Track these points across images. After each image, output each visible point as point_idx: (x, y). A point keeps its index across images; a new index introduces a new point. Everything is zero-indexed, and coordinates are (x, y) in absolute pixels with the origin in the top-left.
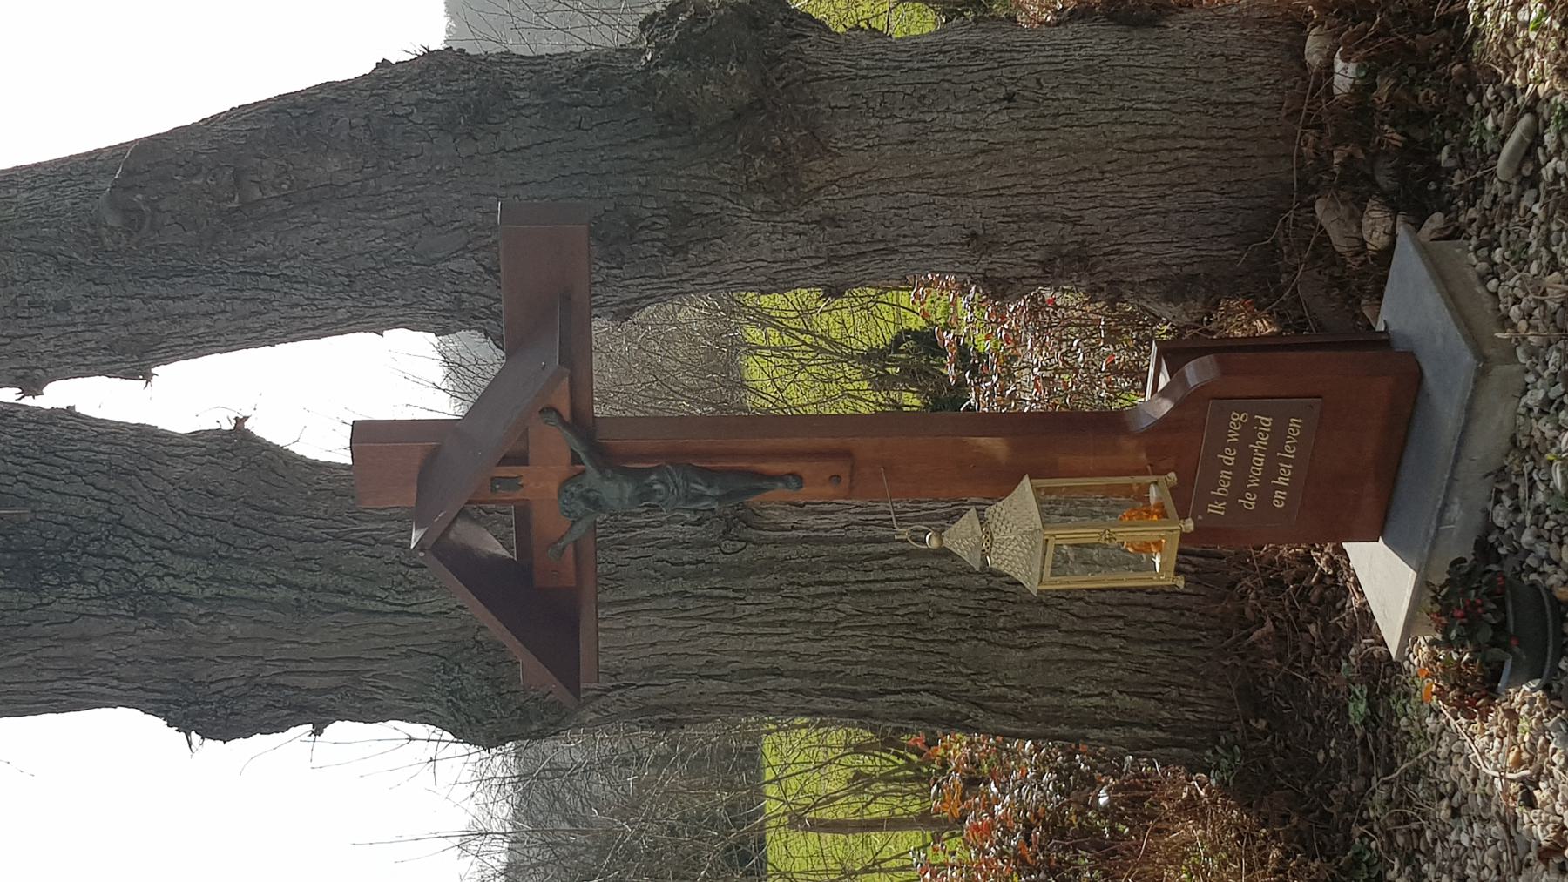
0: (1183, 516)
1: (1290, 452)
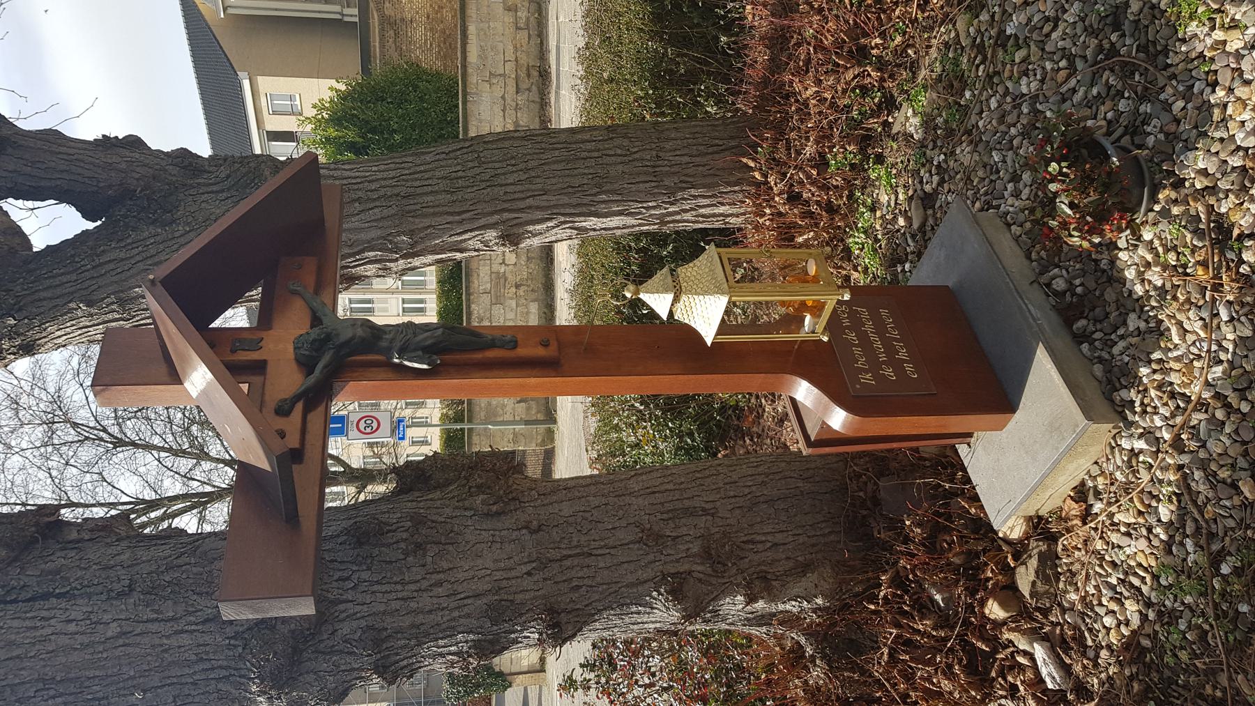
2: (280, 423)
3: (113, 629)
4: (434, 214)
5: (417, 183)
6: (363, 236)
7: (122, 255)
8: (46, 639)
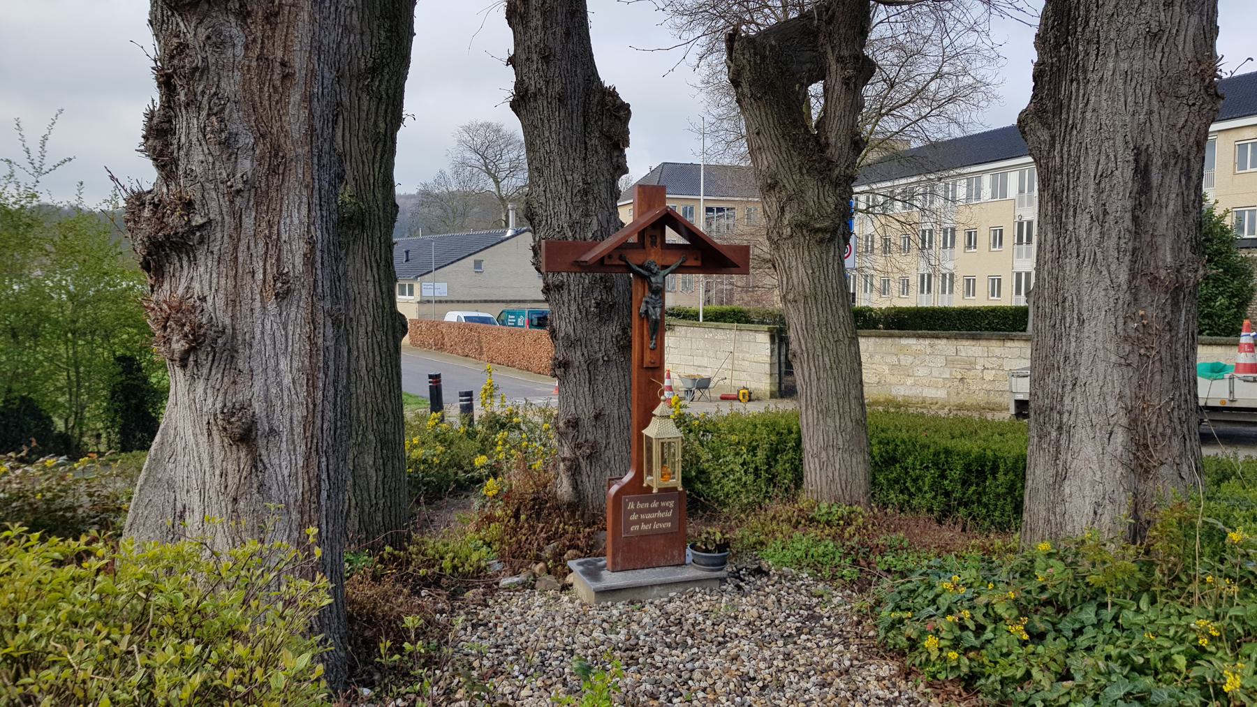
0: (660, 490)
1: (656, 526)
2: (616, 256)
3: (569, 178)
6: (794, 274)
7: (783, 149)
8: (566, 152)
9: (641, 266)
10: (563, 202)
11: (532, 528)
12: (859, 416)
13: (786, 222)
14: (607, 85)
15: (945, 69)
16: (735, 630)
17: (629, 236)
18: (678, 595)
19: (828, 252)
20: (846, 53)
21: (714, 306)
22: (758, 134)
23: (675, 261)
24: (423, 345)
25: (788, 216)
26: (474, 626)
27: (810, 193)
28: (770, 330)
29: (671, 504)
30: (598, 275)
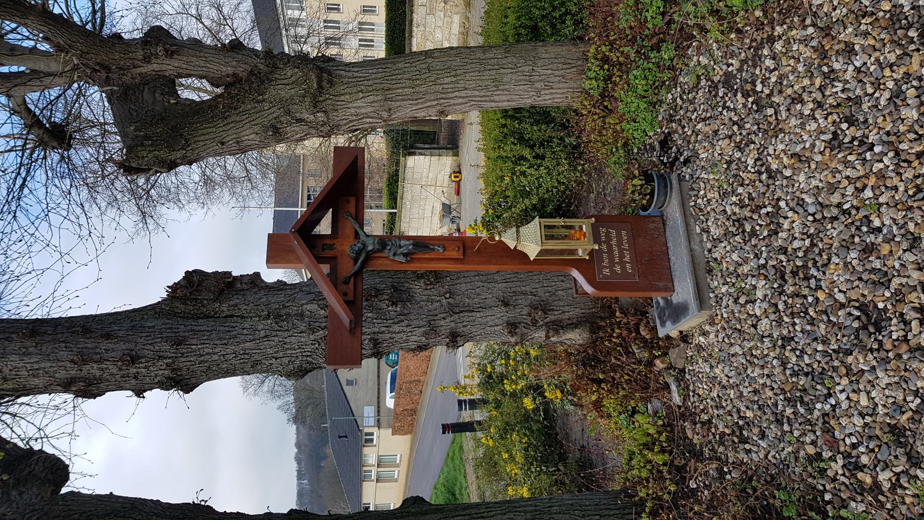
1: (626, 246)
2: (344, 288)
3: (262, 333)
4: (403, 100)
5: (394, 82)
6: (363, 111)
7: (238, 118)
8: (235, 337)
9: (356, 261)
10: (288, 340)
11: (614, 369)
12: (501, 51)
13: (312, 117)
14: (165, 295)
15: (194, 12)
16: (750, 162)
17: (321, 273)
18: (700, 222)
19: (341, 76)
20: (140, 54)
21: (385, 201)
22: (223, 144)
23: (350, 224)
24: (412, 425)
25: (306, 116)
26: (744, 440)
27: (283, 93)
28: (405, 156)
29: (603, 230)
30: (365, 304)
